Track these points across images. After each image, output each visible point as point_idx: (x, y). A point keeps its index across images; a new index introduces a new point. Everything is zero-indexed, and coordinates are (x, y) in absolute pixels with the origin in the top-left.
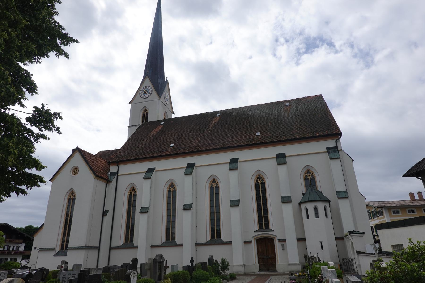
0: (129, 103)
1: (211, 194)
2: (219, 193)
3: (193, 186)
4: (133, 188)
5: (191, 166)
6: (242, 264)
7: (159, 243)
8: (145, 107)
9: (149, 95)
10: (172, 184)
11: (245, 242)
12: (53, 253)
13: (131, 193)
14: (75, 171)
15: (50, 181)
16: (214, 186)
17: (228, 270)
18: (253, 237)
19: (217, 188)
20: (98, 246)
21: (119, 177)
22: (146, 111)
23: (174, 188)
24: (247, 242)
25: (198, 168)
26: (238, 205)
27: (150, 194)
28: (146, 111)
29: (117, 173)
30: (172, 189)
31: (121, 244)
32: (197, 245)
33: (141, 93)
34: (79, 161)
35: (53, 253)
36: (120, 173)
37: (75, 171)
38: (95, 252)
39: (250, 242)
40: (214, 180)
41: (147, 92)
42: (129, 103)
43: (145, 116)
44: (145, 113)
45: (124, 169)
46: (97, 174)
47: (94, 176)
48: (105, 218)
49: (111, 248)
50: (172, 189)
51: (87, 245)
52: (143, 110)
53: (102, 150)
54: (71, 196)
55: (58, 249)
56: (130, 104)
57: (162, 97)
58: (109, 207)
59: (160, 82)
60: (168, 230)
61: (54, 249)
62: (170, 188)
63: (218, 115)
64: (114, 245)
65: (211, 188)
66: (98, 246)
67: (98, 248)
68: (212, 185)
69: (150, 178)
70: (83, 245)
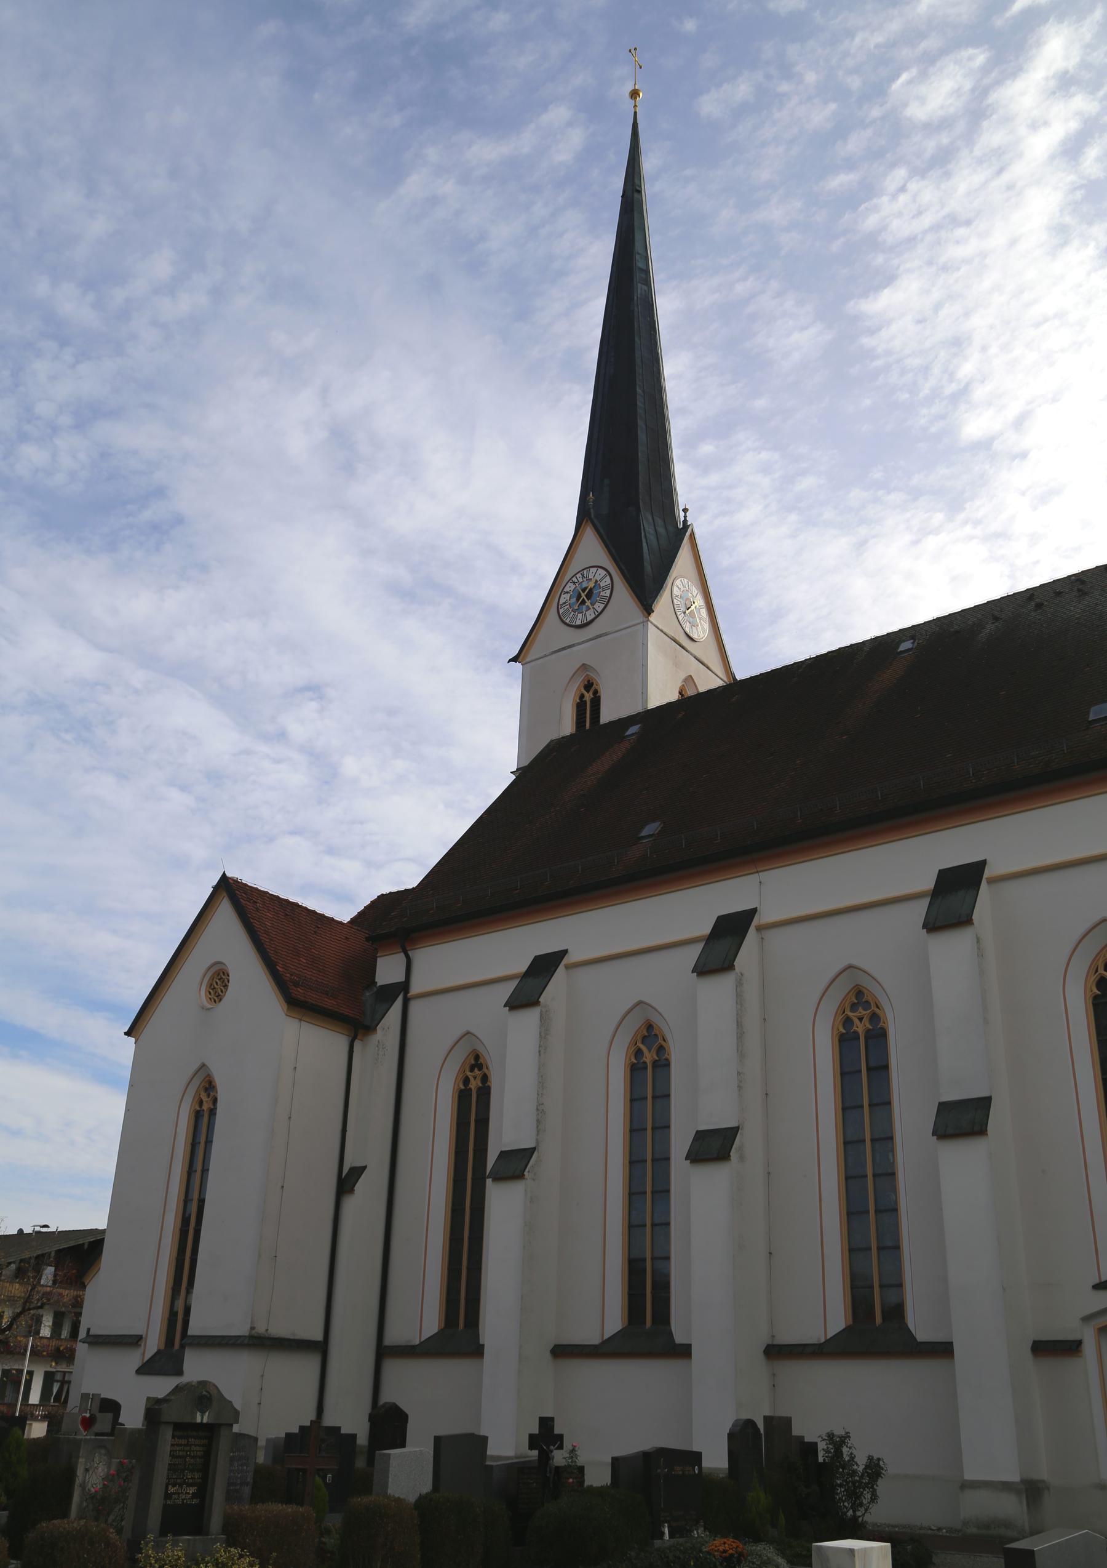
0: (514, 659)
1: (846, 1074)
2: (886, 1067)
3: (741, 1035)
4: (477, 1057)
5: (732, 928)
6: (1014, 1477)
7: (591, 1336)
8: (584, 667)
9: (599, 607)
10: (650, 1026)
11: (1043, 1349)
12: (134, 1359)
13: (466, 1081)
14: (218, 982)
15: (128, 1034)
16: (860, 1028)
17: (354, 1436)
18: (1087, 1319)
19: (878, 1036)
20: (319, 1336)
21: (415, 1007)
22: (589, 686)
23: (661, 1049)
24: (1054, 1349)
25: (769, 934)
26: (978, 1129)
27: (557, 1090)
28: (589, 686)
29: (403, 987)
30: (649, 1057)
31: (425, 1337)
32: (775, 1352)
33: (570, 600)
34: (230, 943)
35: (134, 1359)
36: (415, 988)
37: (218, 982)
38: (309, 1365)
39: (1071, 1348)
40: (859, 992)
41: (589, 595)
42: (514, 659)
43: (588, 704)
44: (588, 696)
45: (440, 963)
46: (299, 993)
47: (285, 1006)
48: (350, 1204)
49: (383, 1352)
50: (649, 1057)
51: (261, 1329)
52: (577, 685)
53: (386, 891)
54: (205, 1099)
55: (153, 1344)
56: (518, 666)
57: (662, 604)
58: (369, 1149)
59: (652, 538)
60: (635, 1269)
61: (134, 1341)
62: (638, 1053)
63: (906, 645)
64: (395, 1335)
65: (845, 1040)
66: (319, 1336)
67: (321, 1348)
68: (848, 1022)
69: (536, 1003)
70: (241, 1329)
